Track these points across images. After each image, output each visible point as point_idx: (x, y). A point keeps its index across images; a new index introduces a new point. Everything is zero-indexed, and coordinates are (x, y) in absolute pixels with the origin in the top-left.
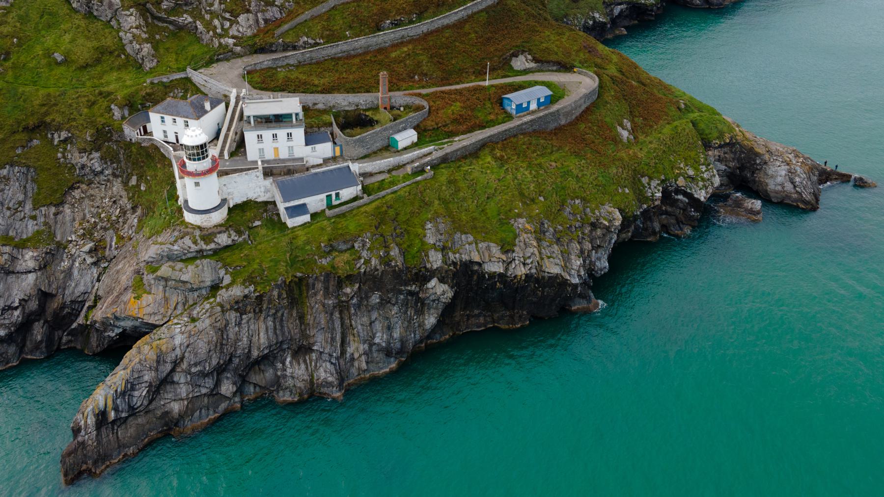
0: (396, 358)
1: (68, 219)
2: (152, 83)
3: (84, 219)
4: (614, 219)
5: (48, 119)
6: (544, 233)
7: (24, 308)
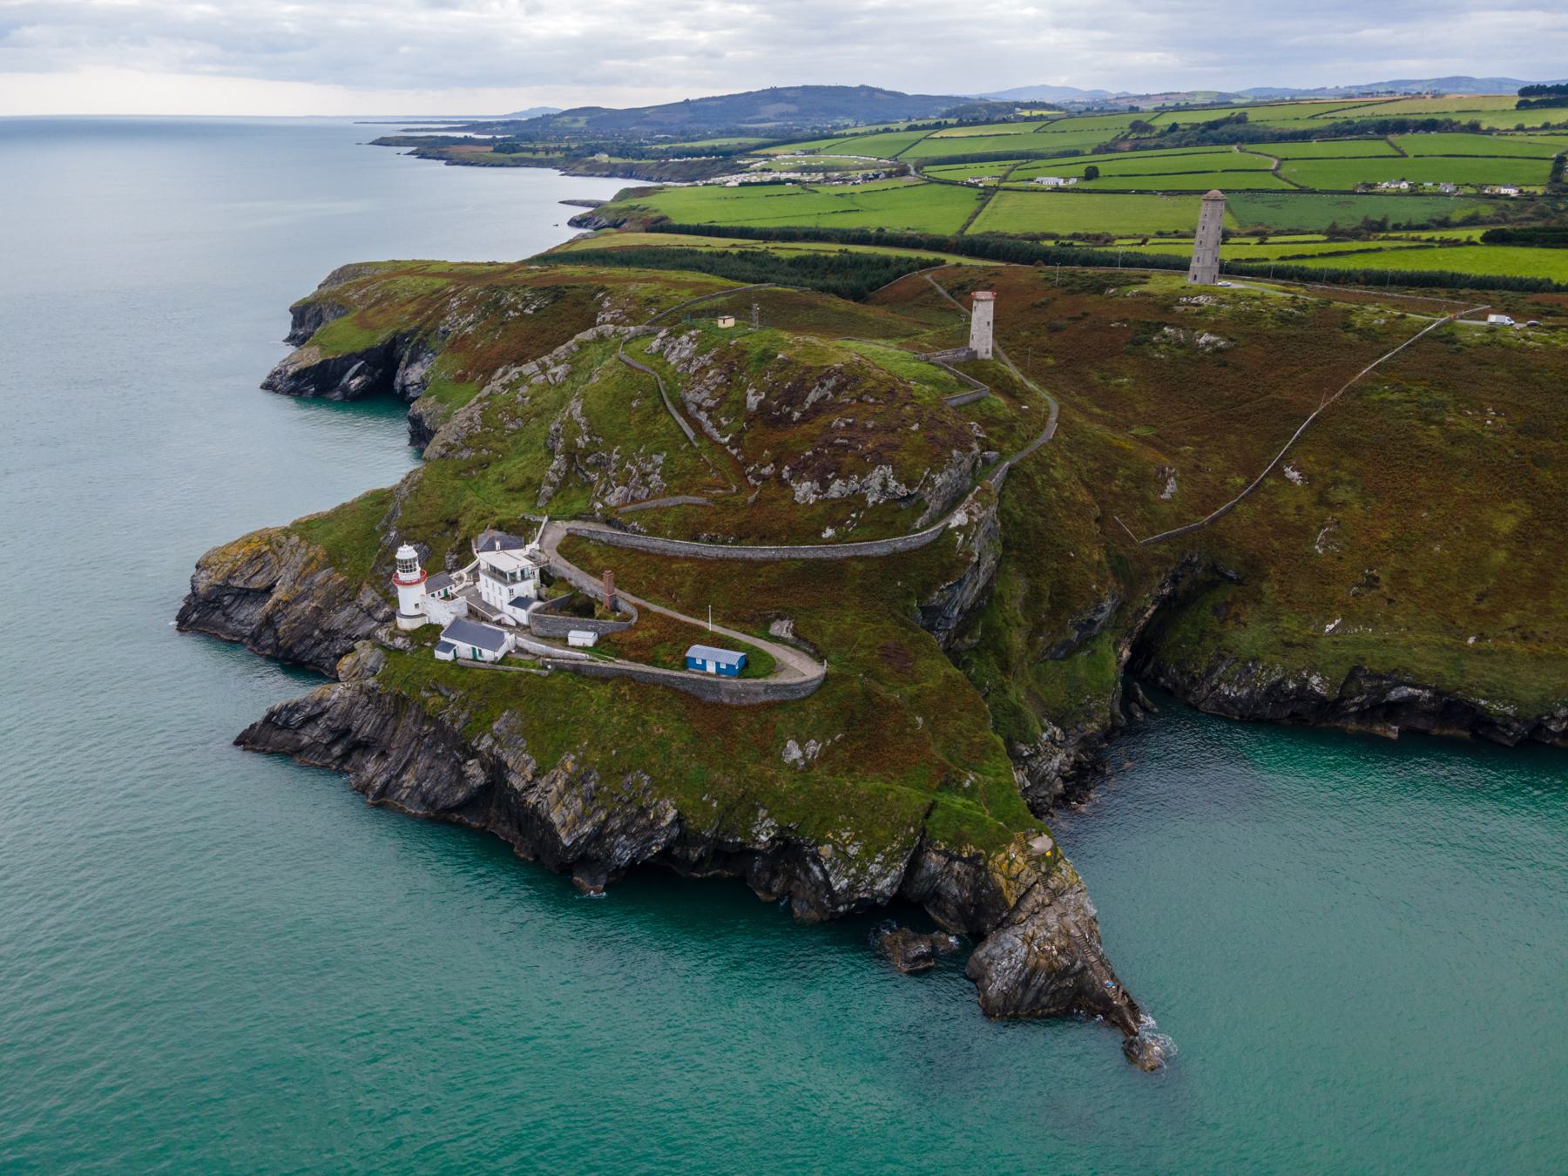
2: (523, 518)
6: (584, 782)
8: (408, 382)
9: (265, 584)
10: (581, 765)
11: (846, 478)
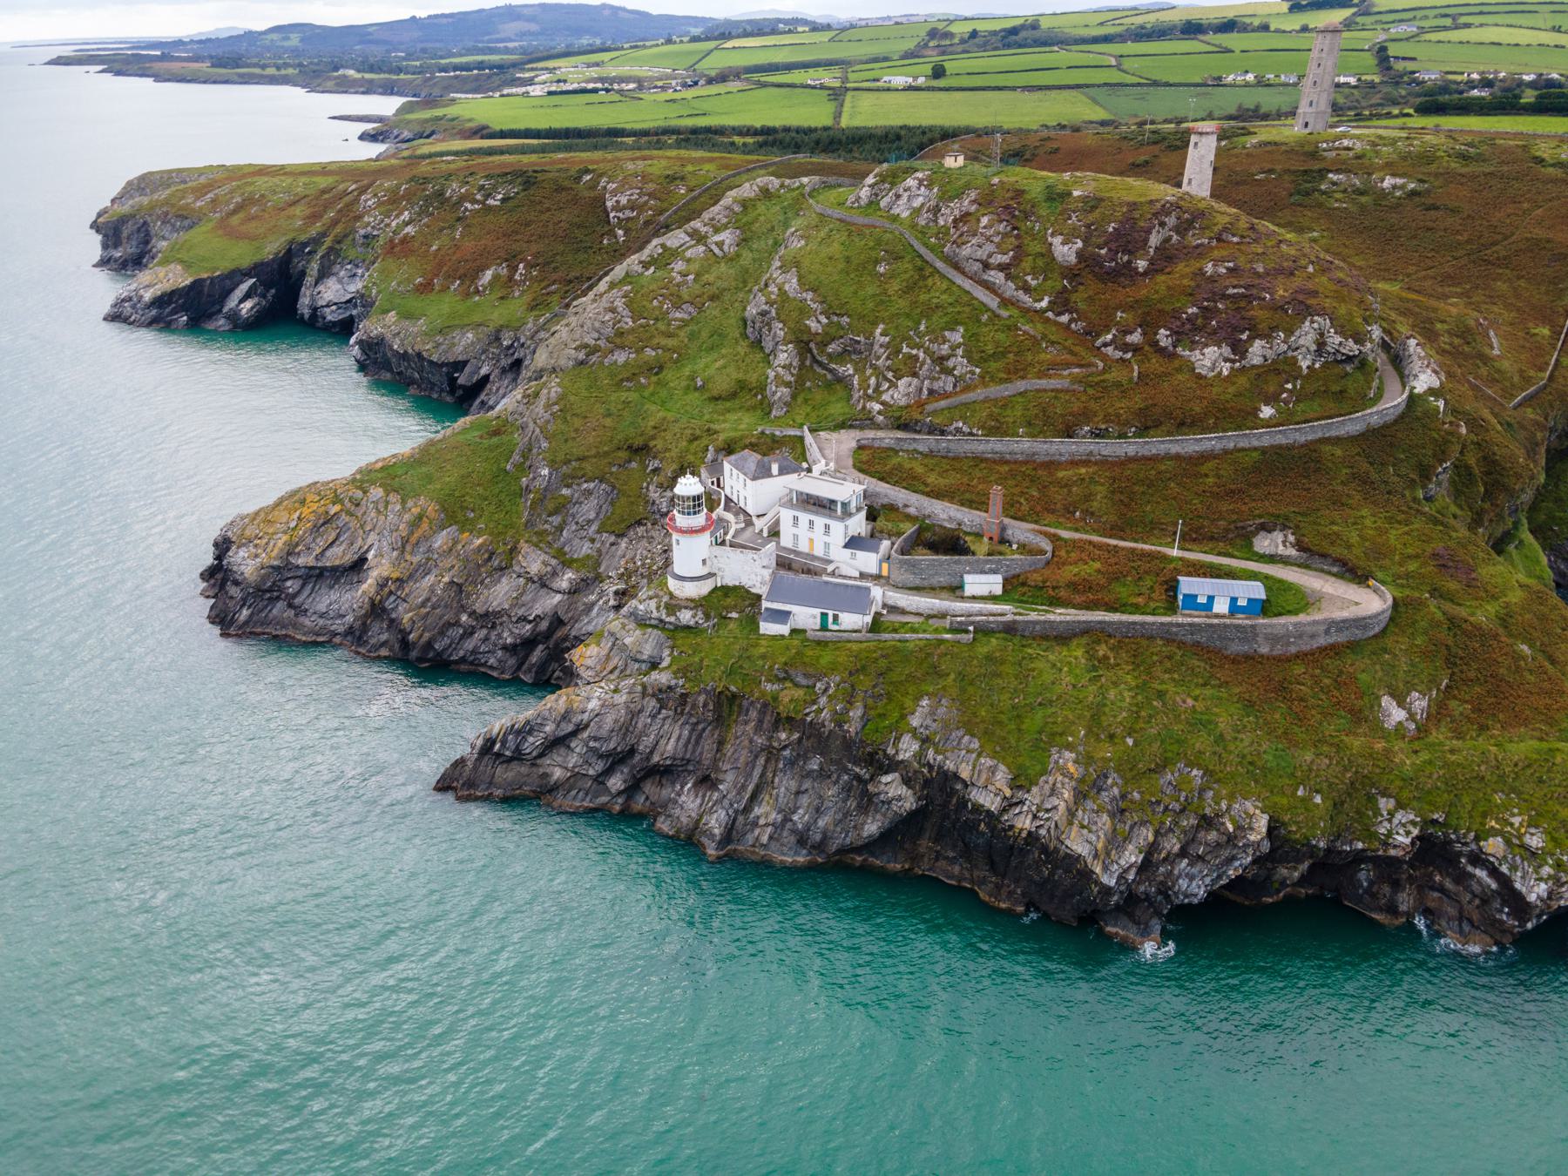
0: (810, 853)
1: (619, 553)
2: (763, 433)
3: (632, 559)
4: (1251, 829)
5: (652, 444)
6: (1100, 790)
7: (536, 625)
8: (321, 303)
9: (349, 558)
10: (1087, 765)
11: (1268, 337)
